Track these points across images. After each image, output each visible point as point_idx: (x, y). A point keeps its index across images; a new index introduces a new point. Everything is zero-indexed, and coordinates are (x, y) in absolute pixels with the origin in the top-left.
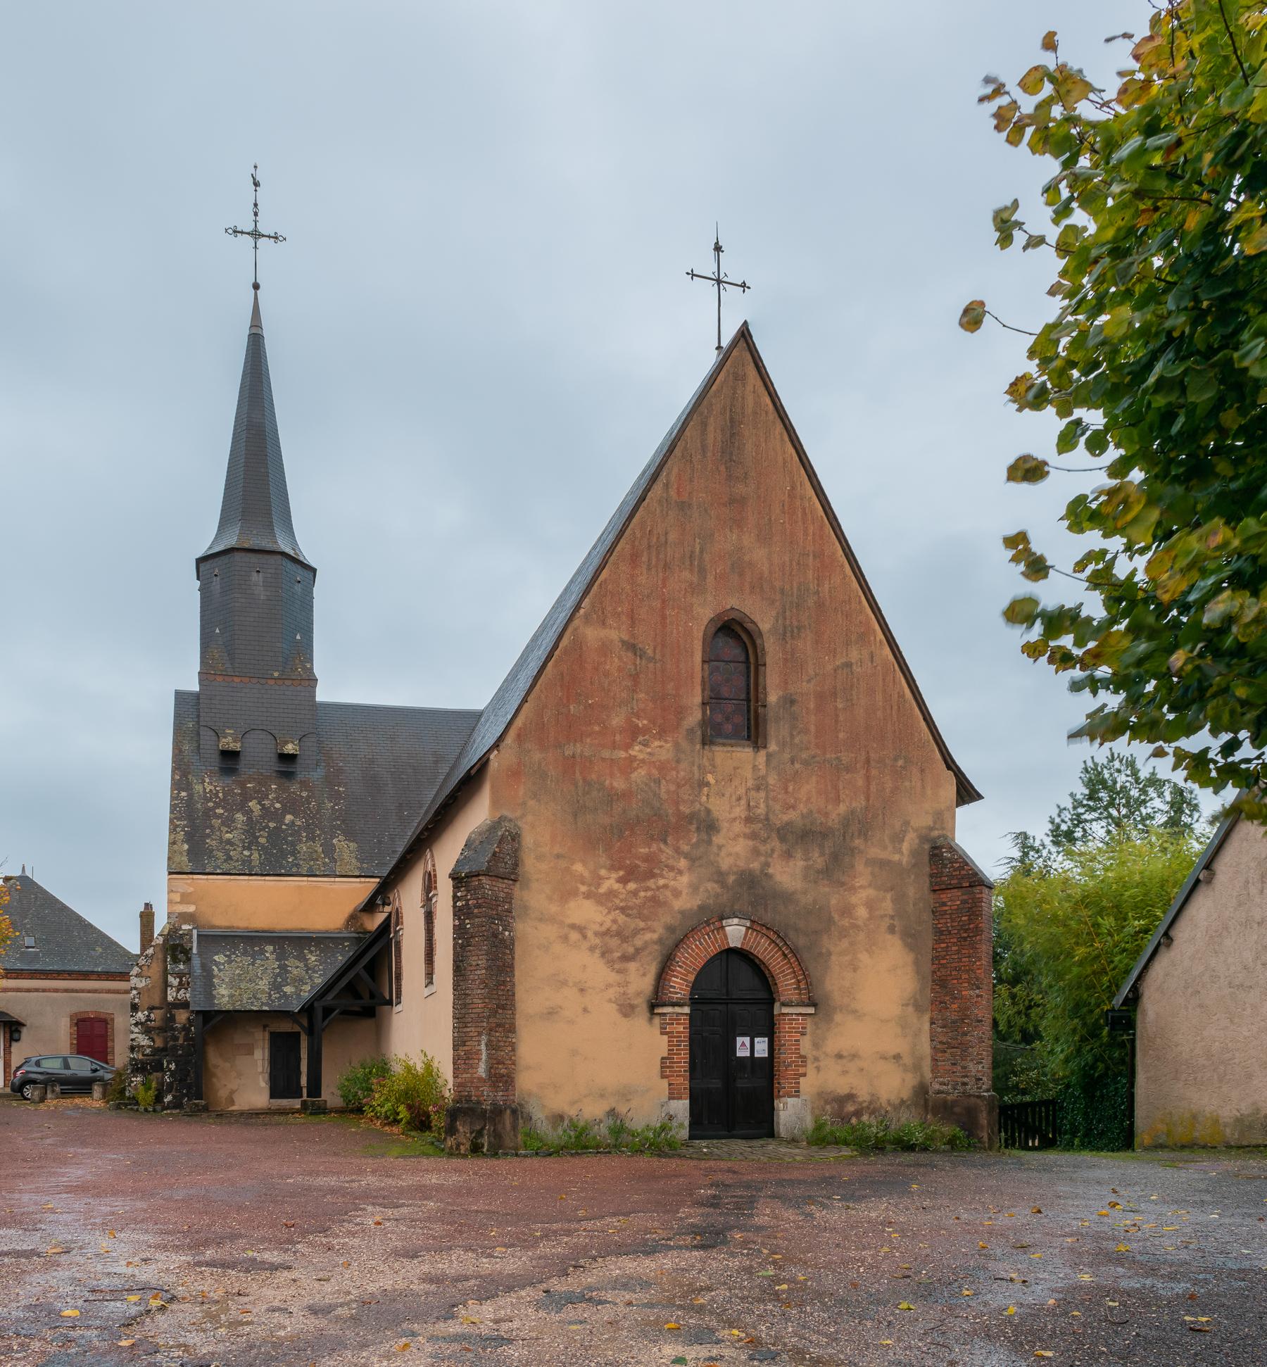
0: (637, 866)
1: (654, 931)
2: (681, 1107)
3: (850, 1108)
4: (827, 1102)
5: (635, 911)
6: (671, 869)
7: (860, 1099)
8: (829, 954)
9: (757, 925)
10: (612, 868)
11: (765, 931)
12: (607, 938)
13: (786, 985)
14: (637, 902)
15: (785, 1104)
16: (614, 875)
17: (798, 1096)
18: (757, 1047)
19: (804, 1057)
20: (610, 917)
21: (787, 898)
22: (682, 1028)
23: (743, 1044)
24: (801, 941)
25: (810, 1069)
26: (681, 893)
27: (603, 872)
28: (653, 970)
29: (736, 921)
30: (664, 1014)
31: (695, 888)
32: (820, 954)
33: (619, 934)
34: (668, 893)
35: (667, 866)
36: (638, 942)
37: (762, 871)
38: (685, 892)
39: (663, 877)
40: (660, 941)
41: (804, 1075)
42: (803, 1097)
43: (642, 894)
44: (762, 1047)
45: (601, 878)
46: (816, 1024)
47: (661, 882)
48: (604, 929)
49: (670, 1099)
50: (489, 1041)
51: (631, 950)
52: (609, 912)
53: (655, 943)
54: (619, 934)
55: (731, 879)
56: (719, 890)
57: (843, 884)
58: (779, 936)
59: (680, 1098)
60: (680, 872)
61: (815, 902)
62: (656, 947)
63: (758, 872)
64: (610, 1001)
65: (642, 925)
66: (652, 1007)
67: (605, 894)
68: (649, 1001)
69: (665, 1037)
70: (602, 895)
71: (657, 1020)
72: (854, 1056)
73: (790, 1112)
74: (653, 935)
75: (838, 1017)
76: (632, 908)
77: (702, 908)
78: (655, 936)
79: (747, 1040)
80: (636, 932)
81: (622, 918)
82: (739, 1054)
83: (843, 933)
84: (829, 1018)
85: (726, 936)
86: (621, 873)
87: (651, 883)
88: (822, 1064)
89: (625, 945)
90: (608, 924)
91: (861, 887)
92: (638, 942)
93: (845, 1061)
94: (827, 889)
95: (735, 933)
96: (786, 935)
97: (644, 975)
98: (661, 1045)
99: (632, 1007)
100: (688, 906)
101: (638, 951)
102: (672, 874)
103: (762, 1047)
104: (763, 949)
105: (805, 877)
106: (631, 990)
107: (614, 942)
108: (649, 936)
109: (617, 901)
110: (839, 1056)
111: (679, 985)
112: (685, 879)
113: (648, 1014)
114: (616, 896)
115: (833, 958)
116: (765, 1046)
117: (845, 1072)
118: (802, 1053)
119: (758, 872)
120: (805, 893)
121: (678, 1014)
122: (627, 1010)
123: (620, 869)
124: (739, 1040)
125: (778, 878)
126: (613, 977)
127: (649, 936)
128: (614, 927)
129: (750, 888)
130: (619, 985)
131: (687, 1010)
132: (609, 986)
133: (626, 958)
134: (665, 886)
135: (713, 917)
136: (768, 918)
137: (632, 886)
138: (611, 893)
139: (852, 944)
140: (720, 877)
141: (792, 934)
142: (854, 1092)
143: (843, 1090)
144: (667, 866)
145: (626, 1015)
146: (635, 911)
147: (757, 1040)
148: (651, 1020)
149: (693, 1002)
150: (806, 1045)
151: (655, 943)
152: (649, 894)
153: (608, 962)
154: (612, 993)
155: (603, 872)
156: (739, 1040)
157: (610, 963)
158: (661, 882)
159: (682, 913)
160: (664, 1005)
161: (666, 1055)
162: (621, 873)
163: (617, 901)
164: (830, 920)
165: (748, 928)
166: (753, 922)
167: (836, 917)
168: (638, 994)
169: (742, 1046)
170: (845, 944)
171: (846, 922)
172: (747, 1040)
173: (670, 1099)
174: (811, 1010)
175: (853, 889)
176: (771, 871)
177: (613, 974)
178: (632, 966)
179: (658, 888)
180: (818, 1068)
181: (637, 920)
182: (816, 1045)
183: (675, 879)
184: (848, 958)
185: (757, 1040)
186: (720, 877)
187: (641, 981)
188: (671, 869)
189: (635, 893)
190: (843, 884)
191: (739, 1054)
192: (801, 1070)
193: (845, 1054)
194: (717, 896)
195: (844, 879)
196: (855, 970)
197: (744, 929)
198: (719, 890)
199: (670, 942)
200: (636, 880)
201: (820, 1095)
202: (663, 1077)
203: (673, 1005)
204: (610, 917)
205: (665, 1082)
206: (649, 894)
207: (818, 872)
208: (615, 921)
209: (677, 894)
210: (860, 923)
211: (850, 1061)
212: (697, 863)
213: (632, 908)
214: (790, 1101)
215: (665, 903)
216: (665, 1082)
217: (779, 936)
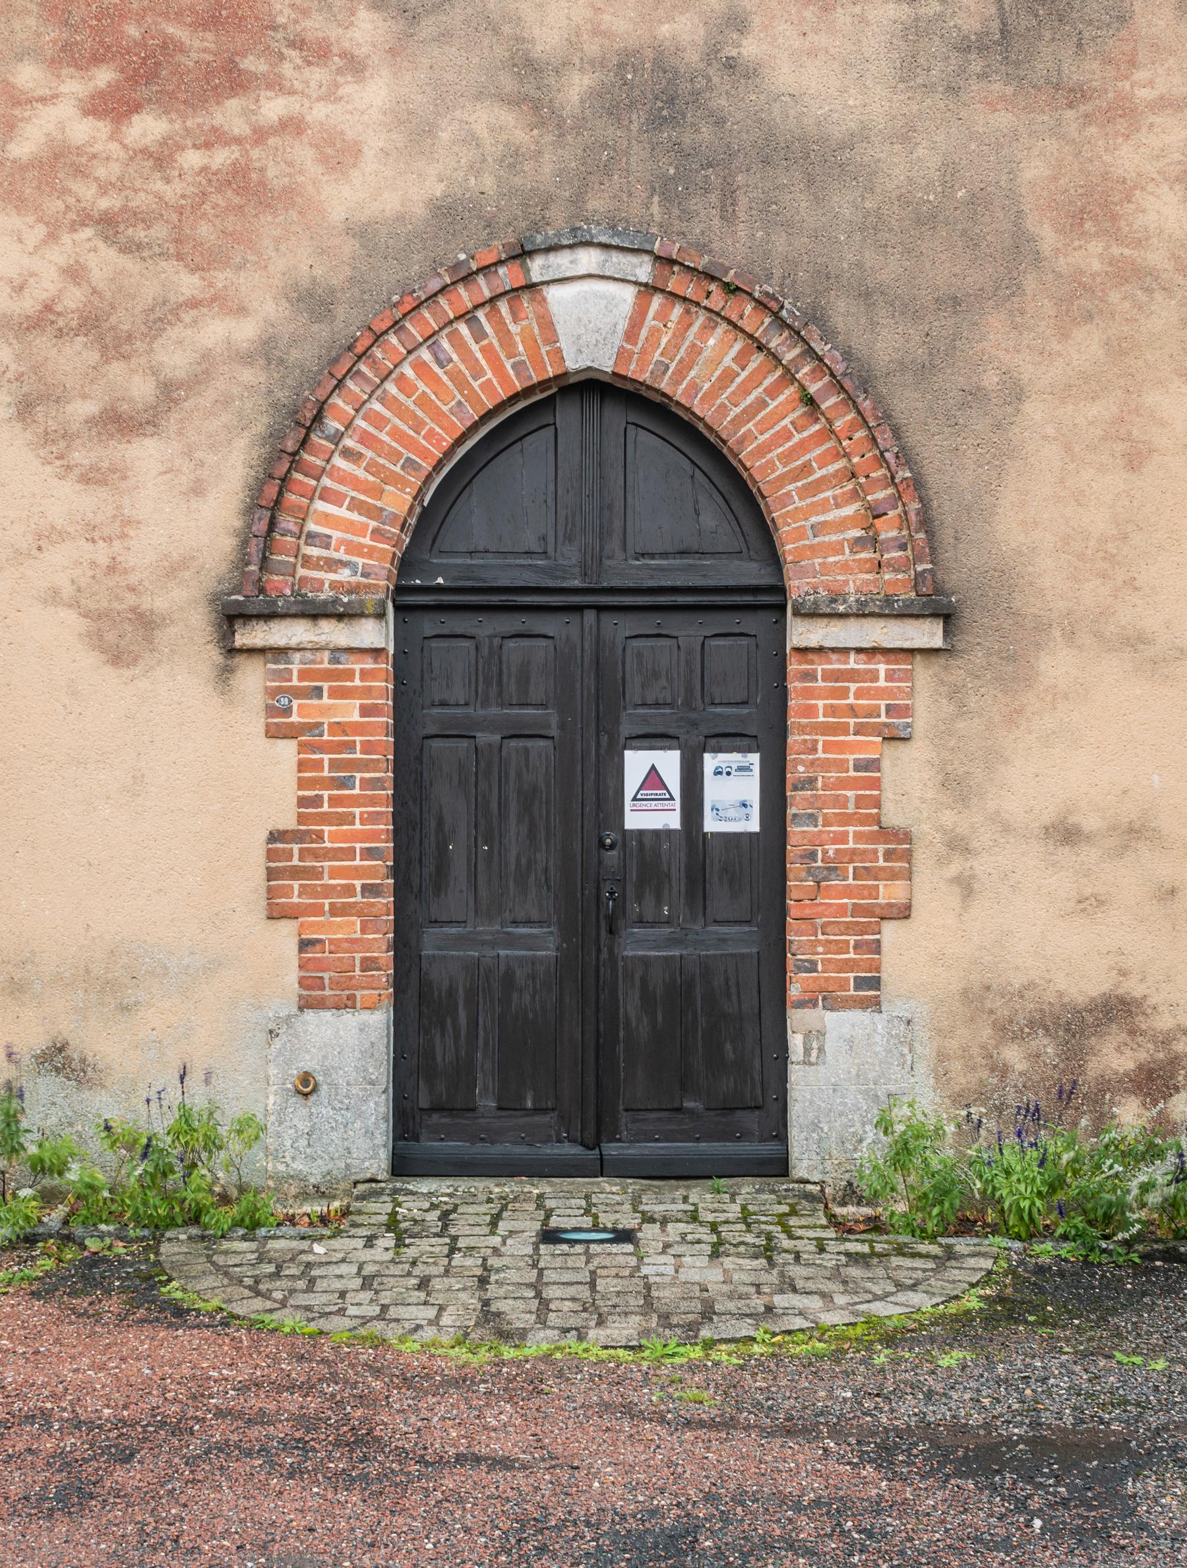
0: (169, 46)
1: (242, 311)
2: (356, 1041)
3: (1114, 1057)
4: (1005, 1031)
5: (160, 232)
6: (318, 52)
7: (1164, 1022)
8: (1015, 393)
9: (684, 278)
10: (69, 57)
11: (717, 300)
12: (43, 343)
13: (821, 532)
14: (172, 191)
15: (816, 1035)
16: (74, 87)
17: (875, 1004)
18: (715, 791)
19: (906, 836)
20: (58, 255)
21: (819, 159)
22: (358, 710)
23: (653, 778)
24: (885, 343)
25: (930, 887)
26: (354, 151)
27: (28, 76)
28: (234, 469)
29: (588, 260)
30: (280, 653)
31: (416, 132)
32: (974, 395)
33: (91, 323)
34: (303, 153)
35: (298, 43)
36: (174, 355)
37: (712, 52)
38: (374, 143)
39: (277, 85)
40: (267, 351)
41: (904, 912)
42: (895, 1007)
43: (192, 159)
44: (733, 794)
45: (20, 100)
46: (955, 693)
47: (273, 108)
48: (28, 305)
49: (305, 1005)
50: (820, 1357)
51: (142, 389)
52: (52, 237)
53: (247, 359)
54: (91, 323)
55: (575, 88)
56: (522, 136)
57: (1077, 95)
58: (779, 318)
59: (349, 1004)
60: (355, 66)
61: (950, 171)
62: (248, 375)
63: (693, 57)
64: (53, 597)
65: (188, 284)
66: (231, 617)
67: (37, 163)
68: (215, 599)
69: (288, 750)
70: (23, 167)
71: (252, 678)
72: (1134, 834)
73: (851, 1078)
74: (234, 327)
75: (1056, 665)
76: (144, 219)
77: (447, 213)
78: (246, 331)
79: (669, 763)
80: (163, 316)
81: (104, 262)
82: (634, 820)
83: (1079, 302)
84: (1015, 667)
85: (547, 325)
86: (104, 76)
87: (230, 114)
88: (981, 865)
89: (116, 369)
90: (47, 284)
91: (1163, 104)
92: (174, 355)
93: (1089, 855)
94: (1004, 119)
95: (589, 314)
96: (816, 316)
97: (198, 490)
98: (272, 781)
99: (147, 623)
100: (390, 203)
101: (170, 392)
102: (318, 75)
103: (733, 794)
104: (706, 370)
105: (908, 71)
106: (143, 551)
107: (71, 359)
108: (216, 331)
109: (86, 191)
110: (1065, 834)
111: (351, 532)
112: (374, 94)
113: (215, 655)
114: (79, 172)
115: (1034, 410)
116: (749, 788)
117: (1090, 904)
118: (893, 816)
119: (693, 57)
120: (906, 135)
121: (338, 652)
122: (123, 635)
123: (96, 60)
124: (636, 763)
125: (784, 76)
126: (67, 501)
127: (216, 331)
128: (74, 298)
129: (657, 122)
130: (91, 532)
131: (374, 634)
132: (47, 537)
133: (119, 422)
134: (292, 126)
135: (502, 259)
136: (733, 247)
137: (148, 127)
138: (60, 161)
139: (1118, 349)
140: (527, 79)
141: (843, 312)
142: (1134, 988)
143: (1086, 983)
144: (298, 43)
145: (117, 658)
146: (160, 232)
147: (711, 761)
148: (225, 673)
149: (409, 602)
150: (909, 785)
151: (247, 359)
152: (222, 157)
153: (47, 438)
154: (61, 565)
155: (28, 76)
156: (636, 763)
157: (55, 443)
158: (273, 108)
159: (362, 232)
160: (270, 616)
161: (288, 820)
162: (104, 76)
163: (86, 191)
164: (1021, 249)
165: (648, 289)
166: (665, 262)
167: (1047, 237)
168: (172, 571)
169: (648, 789)
170: (1086, 347)
171: (1091, 256)
172: (669, 763)
173: (305, 1005)
174: (928, 634)
175: (1124, 114)
176: (750, 48)
177: (68, 488)
178: (146, 454)
179: (260, 135)
180: (966, 886)
181: (169, 267)
182: (955, 786)
183: (331, 95)
184: (1103, 409)
185: (711, 761)
186: (527, 79)
187: (185, 510)
188: (318, 52)
189: (160, 158)
190: (1077, 95)
191: (634, 820)
192: (889, 893)
193: (1090, 822)
194: (513, 158)
195: (1087, 71)
196: (1134, 461)
197: (628, 294)
198: (522, 136)
199: (306, 355)
200: (166, 102)
201: (974, 999)
202: (276, 914)
203: (315, 613)
204: (58, 255)
205: (286, 934)
206: (222, 157)
207: (964, 47)
208: (74, 273)
209: (339, 154)
210: (1156, 257)
211: (1121, 851)
212: (428, 27)
213: (144, 219)
214: (839, 1024)
215: (290, 194)
216: (286, 934)
217: (779, 318)
